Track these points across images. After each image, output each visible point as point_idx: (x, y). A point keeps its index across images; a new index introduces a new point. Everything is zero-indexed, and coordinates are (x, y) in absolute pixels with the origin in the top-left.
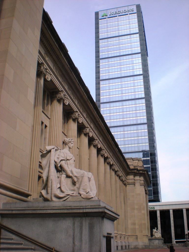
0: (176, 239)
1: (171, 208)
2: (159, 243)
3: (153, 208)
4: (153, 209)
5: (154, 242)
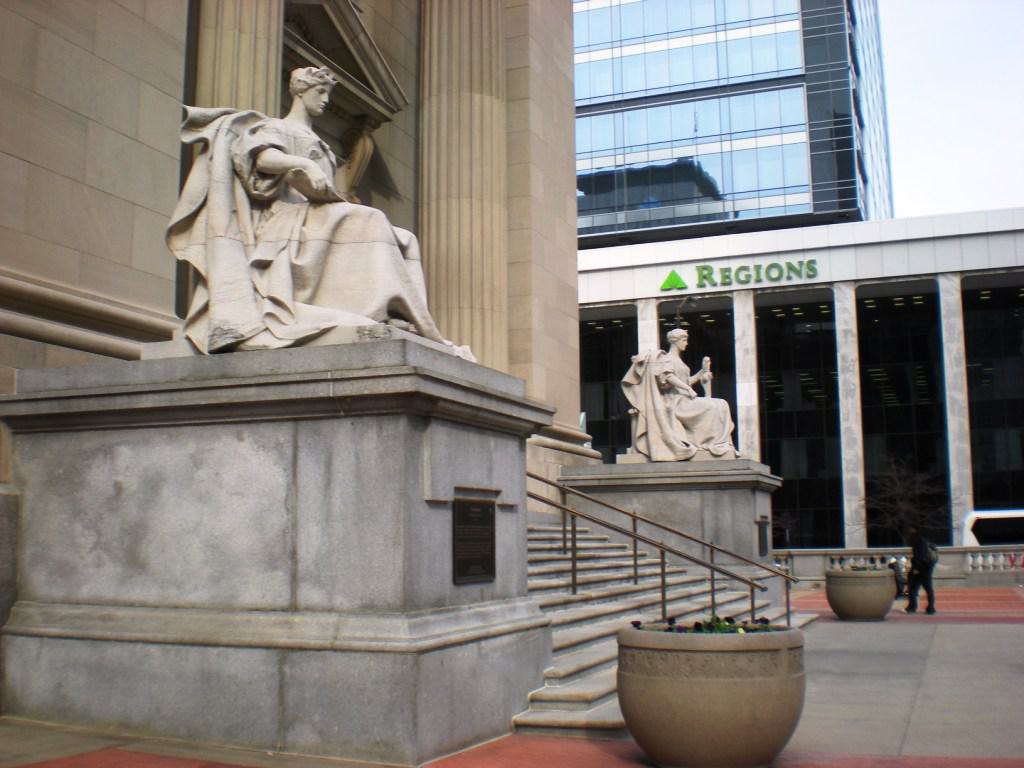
0: (979, 505)
1: (947, 265)
2: (311, 541)
3: (804, 271)
4: (804, 281)
5: (153, 485)
